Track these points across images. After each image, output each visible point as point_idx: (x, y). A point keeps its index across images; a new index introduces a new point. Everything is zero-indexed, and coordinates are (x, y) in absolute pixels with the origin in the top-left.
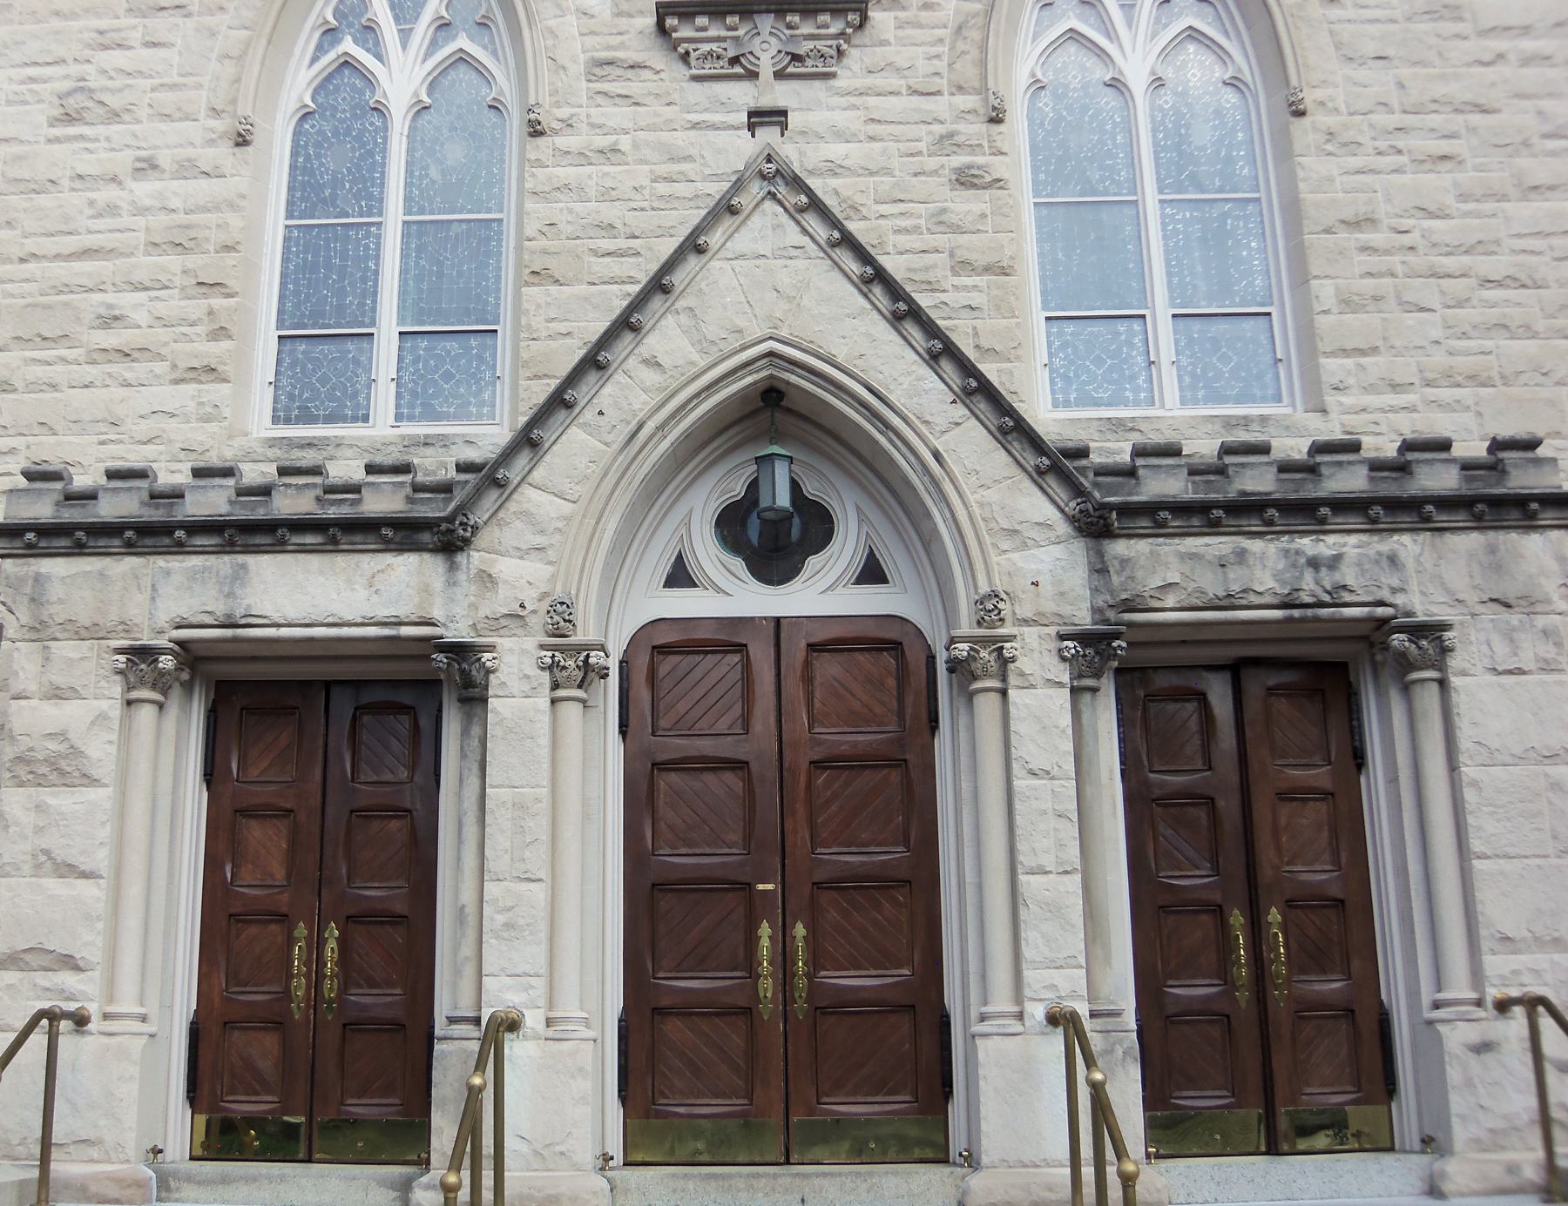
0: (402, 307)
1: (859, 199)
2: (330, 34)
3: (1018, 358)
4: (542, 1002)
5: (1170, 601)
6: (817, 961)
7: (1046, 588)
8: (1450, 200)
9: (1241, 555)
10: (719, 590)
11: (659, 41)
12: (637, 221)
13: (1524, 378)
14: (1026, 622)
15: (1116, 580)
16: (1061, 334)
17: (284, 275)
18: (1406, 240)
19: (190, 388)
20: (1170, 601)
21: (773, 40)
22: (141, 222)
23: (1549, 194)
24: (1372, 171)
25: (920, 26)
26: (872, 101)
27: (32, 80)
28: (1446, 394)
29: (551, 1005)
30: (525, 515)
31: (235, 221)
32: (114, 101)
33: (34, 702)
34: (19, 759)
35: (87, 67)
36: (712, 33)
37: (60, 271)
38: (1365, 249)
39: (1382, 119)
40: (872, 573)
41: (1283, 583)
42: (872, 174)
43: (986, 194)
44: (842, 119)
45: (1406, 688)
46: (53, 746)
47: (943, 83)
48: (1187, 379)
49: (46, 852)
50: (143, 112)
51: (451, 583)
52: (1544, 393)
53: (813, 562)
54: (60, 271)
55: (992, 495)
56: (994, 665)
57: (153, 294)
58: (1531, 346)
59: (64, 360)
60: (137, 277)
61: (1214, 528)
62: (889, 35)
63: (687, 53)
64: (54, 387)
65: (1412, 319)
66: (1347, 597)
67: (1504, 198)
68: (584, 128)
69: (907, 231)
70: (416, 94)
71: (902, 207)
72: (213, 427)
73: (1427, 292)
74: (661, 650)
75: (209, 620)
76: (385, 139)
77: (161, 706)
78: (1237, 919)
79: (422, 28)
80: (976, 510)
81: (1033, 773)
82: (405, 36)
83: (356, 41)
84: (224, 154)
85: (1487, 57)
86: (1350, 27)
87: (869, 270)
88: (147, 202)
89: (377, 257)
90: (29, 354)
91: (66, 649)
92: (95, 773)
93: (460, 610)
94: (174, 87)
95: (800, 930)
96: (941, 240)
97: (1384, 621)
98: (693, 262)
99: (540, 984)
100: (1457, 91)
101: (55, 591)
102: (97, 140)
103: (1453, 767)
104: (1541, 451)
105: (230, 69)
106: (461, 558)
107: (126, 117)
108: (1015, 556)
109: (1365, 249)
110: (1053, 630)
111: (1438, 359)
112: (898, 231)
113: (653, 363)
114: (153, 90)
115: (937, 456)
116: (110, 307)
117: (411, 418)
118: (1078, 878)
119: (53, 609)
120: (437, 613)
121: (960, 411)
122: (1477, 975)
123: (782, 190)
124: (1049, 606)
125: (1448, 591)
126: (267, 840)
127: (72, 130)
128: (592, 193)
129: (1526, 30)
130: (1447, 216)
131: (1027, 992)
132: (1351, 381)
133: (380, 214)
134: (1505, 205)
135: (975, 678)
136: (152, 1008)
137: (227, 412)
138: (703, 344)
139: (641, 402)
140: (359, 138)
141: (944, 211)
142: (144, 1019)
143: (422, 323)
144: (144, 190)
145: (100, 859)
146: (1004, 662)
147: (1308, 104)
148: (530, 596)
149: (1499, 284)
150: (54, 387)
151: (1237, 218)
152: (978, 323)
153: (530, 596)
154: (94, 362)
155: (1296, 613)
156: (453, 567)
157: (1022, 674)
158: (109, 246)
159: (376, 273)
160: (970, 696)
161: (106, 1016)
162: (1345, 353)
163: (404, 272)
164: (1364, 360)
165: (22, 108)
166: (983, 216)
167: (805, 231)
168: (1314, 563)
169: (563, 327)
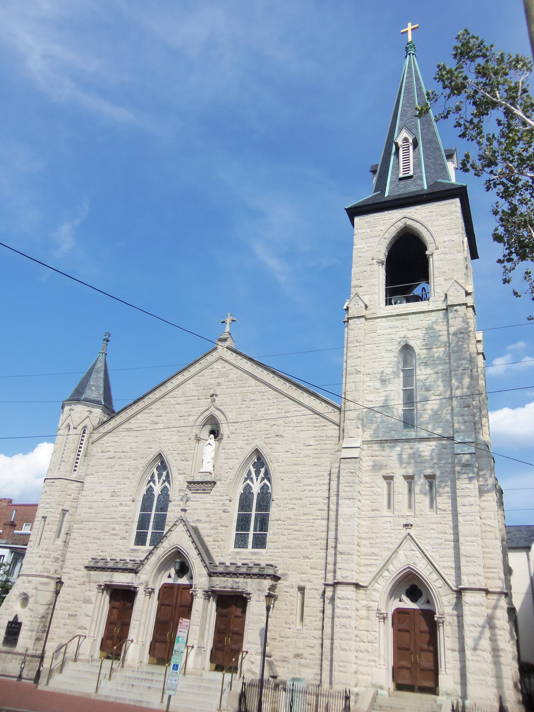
1: (209, 514)
2: (246, 479)
7: (203, 584)
15: (211, 583)
18: (284, 523)
19: (122, 540)
25: (223, 484)
28: (284, 550)
31: (131, 514)
32: (118, 494)
38: (278, 524)
39: (285, 501)
47: (225, 494)
50: (122, 495)
51: (136, 578)
53: (419, 600)
55: (199, 569)
58: (299, 542)
61: (224, 576)
64: (105, 539)
71: (215, 515)
73: (286, 532)
74: (165, 587)
79: (260, 479)
91: (92, 584)
93: (136, 582)
94: (126, 491)
98: (170, 532)
100: (297, 496)
101: (92, 576)
109: (278, 524)
110: (202, 590)
111: (285, 544)
113: (163, 547)
116: (114, 527)
120: (133, 582)
124: (202, 586)
126: (115, 612)
127: (113, 498)
129: (310, 485)
132: (272, 547)
136: (95, 635)
137: (126, 544)
141: (220, 516)
144: (120, 508)
149: (297, 531)
150: (105, 539)
155: (233, 590)
156: (136, 576)
161: (89, 636)
162: (272, 542)
164: (274, 544)
168: (236, 582)
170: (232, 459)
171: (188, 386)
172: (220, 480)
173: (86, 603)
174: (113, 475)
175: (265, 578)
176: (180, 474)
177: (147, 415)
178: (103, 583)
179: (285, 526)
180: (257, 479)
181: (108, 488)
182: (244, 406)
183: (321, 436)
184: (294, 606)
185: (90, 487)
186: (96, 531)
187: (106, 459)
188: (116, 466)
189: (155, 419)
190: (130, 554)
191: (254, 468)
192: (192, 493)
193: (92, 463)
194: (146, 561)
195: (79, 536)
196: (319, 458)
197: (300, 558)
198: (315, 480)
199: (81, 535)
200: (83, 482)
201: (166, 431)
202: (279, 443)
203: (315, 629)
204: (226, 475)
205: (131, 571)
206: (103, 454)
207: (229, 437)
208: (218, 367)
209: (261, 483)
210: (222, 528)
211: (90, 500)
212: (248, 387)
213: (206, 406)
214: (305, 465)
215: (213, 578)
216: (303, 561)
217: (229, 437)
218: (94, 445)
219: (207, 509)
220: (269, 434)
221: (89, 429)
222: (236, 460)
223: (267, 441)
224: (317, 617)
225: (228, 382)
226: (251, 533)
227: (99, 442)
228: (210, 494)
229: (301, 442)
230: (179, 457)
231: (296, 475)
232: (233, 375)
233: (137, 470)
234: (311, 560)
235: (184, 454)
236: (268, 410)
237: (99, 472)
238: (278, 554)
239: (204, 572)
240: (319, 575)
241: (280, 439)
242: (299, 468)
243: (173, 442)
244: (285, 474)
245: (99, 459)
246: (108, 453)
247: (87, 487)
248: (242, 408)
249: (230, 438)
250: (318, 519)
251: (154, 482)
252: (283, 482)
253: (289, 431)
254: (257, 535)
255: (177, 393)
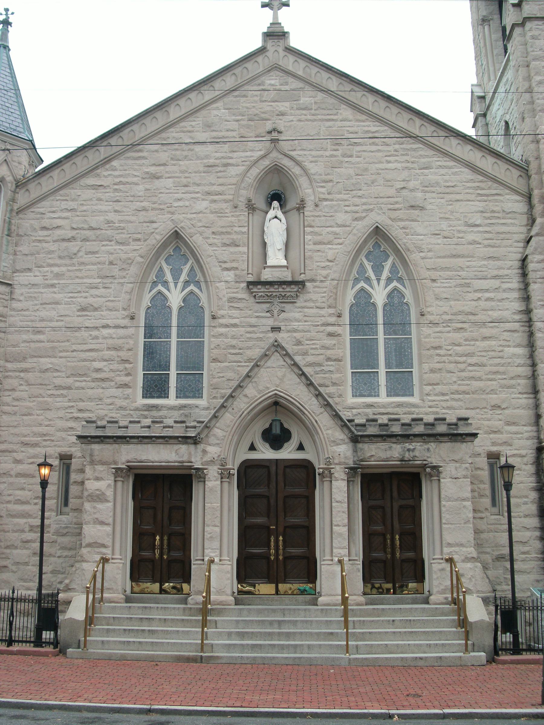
0: (177, 366)
1: (302, 340)
3: (342, 385)
4: (219, 556)
5: (373, 459)
6: (285, 547)
8: (462, 341)
9: (390, 448)
10: (262, 452)
11: (248, 291)
12: (241, 345)
13: (478, 392)
14: (336, 464)
15: (359, 454)
16: (355, 376)
17: (144, 355)
18: (450, 353)
19: (120, 390)
20: (373, 459)
21: (278, 306)
22: (105, 341)
23: (489, 339)
24: (441, 332)
26: (306, 310)
27: (72, 297)
28: (456, 396)
29: (221, 556)
30: (214, 435)
31: (131, 342)
33: (92, 481)
34: (89, 495)
35: (87, 294)
36: (262, 290)
37: (84, 355)
38: (438, 355)
40: (301, 447)
41: (401, 455)
42: (305, 332)
43: (336, 338)
44: (297, 315)
45: (431, 481)
46: (98, 492)
48: (389, 390)
49: (97, 519)
50: (104, 308)
52: (483, 396)
53: (286, 445)
54: (84, 355)
55: (330, 432)
56: (328, 475)
57: (109, 362)
59: (85, 381)
60: (105, 357)
62: (311, 290)
63: (255, 296)
64: (83, 388)
65: (449, 375)
66: (416, 459)
67: (477, 340)
68: (227, 317)
69: (314, 349)
70: (179, 303)
71: (313, 342)
72: (127, 401)
74: (248, 467)
75: (135, 461)
76: (171, 315)
77: (123, 481)
78: (388, 536)
80: (325, 435)
81: (337, 502)
82: (176, 284)
83: (162, 285)
84: (126, 322)
85: (476, 299)
86: (438, 289)
87: (301, 372)
88: (106, 335)
89: (170, 351)
90: (75, 379)
91: (100, 468)
92: (108, 499)
95: (281, 538)
96: (322, 351)
97: (426, 465)
99: (218, 551)
100: (467, 309)
101: (96, 453)
102: (91, 316)
103: (440, 501)
104: (469, 421)
105: (128, 297)
106: (198, 446)
107: (99, 310)
108: (334, 447)
109: (438, 355)
111: (455, 387)
112: (312, 349)
114: (106, 302)
115: (316, 421)
117: (180, 398)
118: (347, 527)
119: (96, 457)
120: (193, 460)
121: (323, 410)
122: (442, 553)
123: (279, 349)
124: (343, 460)
125: (441, 457)
128: (229, 336)
130: (461, 346)
131: (334, 555)
133: (170, 338)
134: (477, 342)
135: (324, 477)
137: (131, 397)
138: (260, 391)
139: (243, 406)
140: (164, 315)
142: (121, 559)
143: (183, 370)
145: (111, 520)
146: (331, 474)
147: (426, 313)
148: (216, 456)
149: (473, 365)
151: (405, 343)
152: (332, 375)
153: (216, 456)
154: (94, 382)
155: (403, 463)
156: (196, 448)
157: (335, 477)
158: (97, 348)
159: (170, 355)
160: (323, 481)
161: (112, 559)
163: (177, 355)
164: (435, 387)
165: (69, 306)
166: (335, 345)
167: (285, 361)
168: (409, 450)
169: (221, 375)
170: (329, 243)
171: (215, 112)
172: (312, 280)
173: (94, 501)
174: (76, 270)
175: (128, 443)
176: (227, 269)
177: (133, 162)
178: (124, 464)
179: (450, 358)
180: (378, 280)
181: (71, 295)
182: (338, 153)
183: (493, 211)
184: (484, 484)
185: (28, 293)
186: (59, 374)
187: (54, 241)
188: (81, 254)
189: (152, 169)
190: (142, 413)
191: (369, 260)
192: (257, 303)
193: (24, 248)
194: (213, 422)
195: (21, 385)
196: (497, 247)
197: (485, 408)
198: (496, 283)
199: (27, 381)
200: (10, 285)
201: (180, 191)
202: (419, 219)
203: (526, 516)
204: (324, 272)
205: (185, 440)
206: (45, 233)
207: (317, 206)
208: (273, 82)
209: (386, 287)
210: (329, 363)
211: (32, 318)
212: (341, 121)
213: (260, 150)
214: (473, 257)
215: (360, 445)
216: (491, 412)
217: (317, 206)
218: (21, 216)
219: (295, 331)
220: (397, 203)
221: (9, 185)
222: (339, 246)
223: (394, 214)
224: (526, 497)
225: (298, 109)
226: (382, 370)
227: (32, 210)
228: (296, 305)
229: (459, 220)
230: (217, 240)
231: (460, 273)
232: (307, 99)
233: (130, 261)
234: (506, 411)
235: (228, 233)
236: (389, 162)
237: (44, 265)
238: (445, 404)
239: (340, 435)
240: (522, 434)
241: (417, 212)
242: (460, 262)
243: (201, 212)
244: (438, 271)
245: (40, 241)
246: (58, 232)
247: (22, 294)
248: (335, 156)
249: (321, 207)
250: (509, 346)
251: (165, 283)
252: (435, 284)
253: (433, 201)
254: (392, 374)
255: (193, 123)
